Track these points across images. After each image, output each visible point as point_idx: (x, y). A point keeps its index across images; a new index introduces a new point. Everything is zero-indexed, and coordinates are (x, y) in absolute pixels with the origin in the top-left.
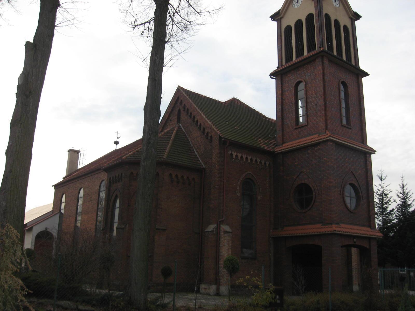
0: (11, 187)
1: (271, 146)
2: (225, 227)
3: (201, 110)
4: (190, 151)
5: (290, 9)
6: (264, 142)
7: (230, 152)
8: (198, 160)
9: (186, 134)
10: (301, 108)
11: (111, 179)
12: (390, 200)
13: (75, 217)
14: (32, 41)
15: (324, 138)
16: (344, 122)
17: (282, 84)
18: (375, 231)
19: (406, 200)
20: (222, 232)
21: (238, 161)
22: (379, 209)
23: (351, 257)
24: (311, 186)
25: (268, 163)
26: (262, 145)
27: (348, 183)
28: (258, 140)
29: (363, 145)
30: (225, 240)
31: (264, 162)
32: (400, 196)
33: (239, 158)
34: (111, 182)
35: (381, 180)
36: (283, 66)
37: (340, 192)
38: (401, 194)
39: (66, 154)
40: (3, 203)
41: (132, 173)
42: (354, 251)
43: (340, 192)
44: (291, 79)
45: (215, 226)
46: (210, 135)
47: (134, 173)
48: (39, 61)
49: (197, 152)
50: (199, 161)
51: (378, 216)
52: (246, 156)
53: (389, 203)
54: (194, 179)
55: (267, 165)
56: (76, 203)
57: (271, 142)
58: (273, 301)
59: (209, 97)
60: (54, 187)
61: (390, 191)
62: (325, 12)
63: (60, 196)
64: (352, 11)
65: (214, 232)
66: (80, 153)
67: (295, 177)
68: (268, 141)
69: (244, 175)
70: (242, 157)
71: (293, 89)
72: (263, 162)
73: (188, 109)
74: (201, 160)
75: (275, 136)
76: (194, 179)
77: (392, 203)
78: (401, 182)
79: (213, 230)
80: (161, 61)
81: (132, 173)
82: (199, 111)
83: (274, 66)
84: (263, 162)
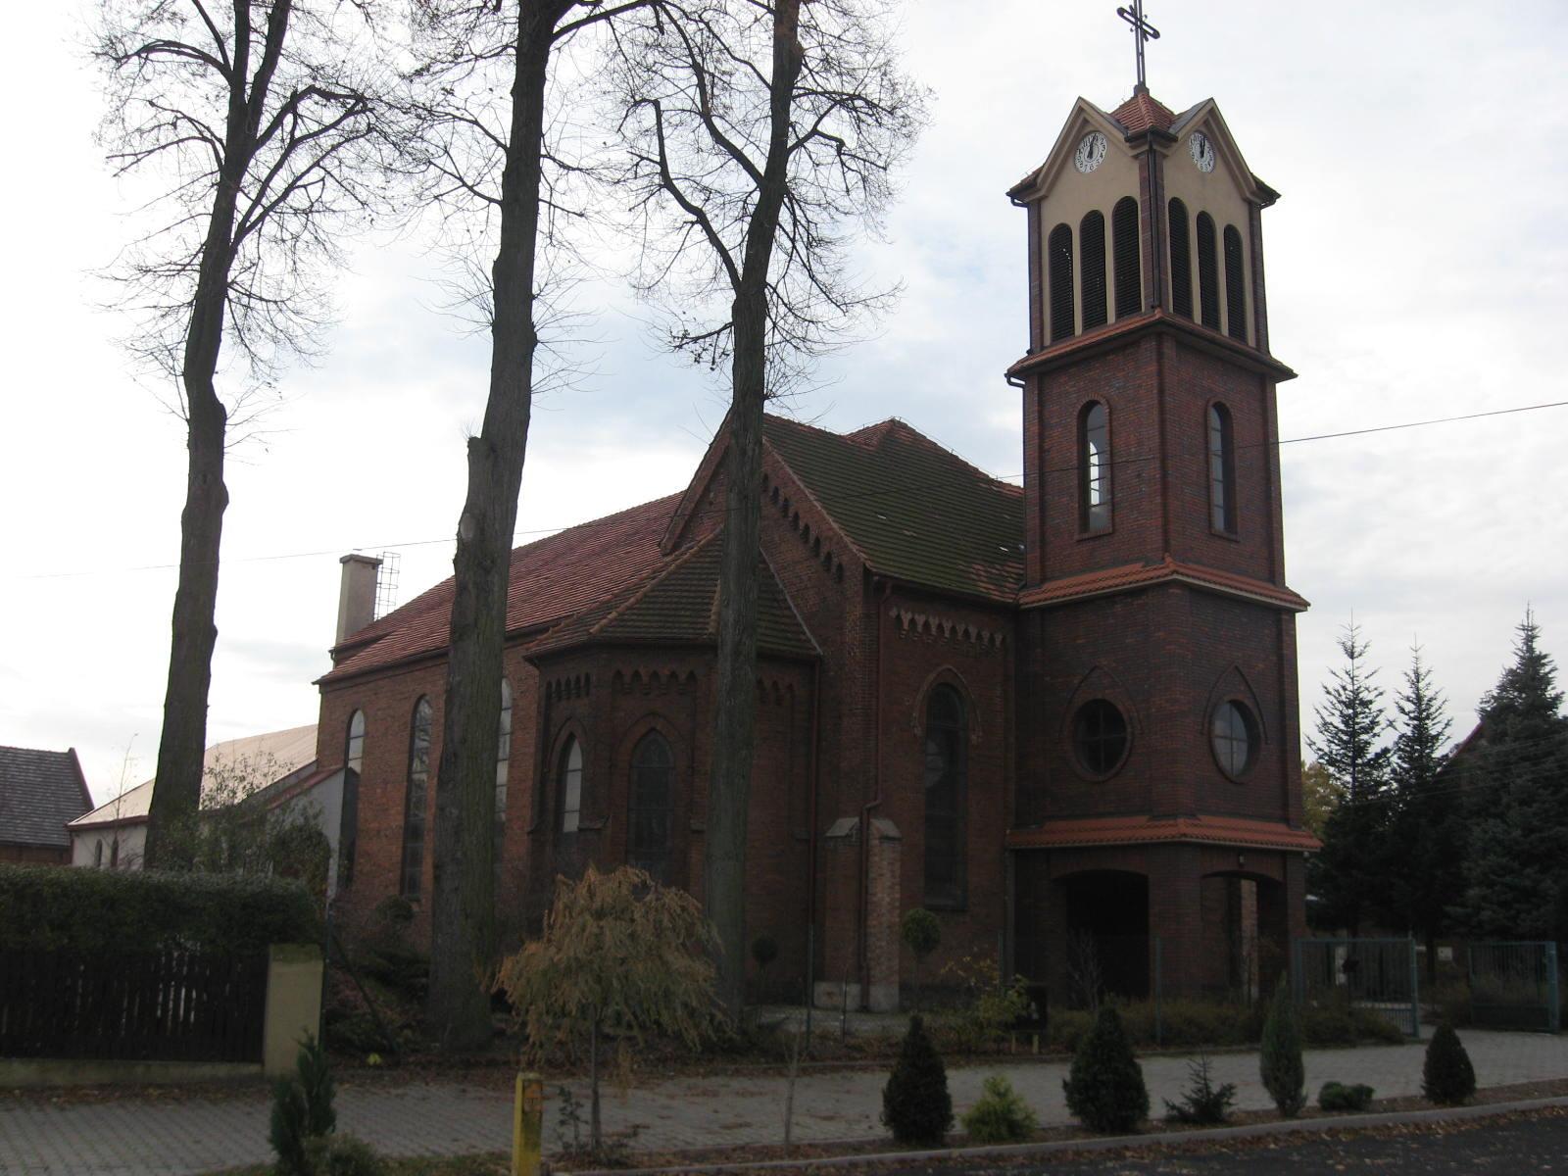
0: (467, 775)
1: (1008, 585)
2: (883, 826)
3: (809, 485)
4: (776, 604)
5: (1068, 175)
6: (988, 572)
7: (893, 613)
10: (1097, 482)
12: (1377, 720)
14: (479, 436)
15: (1159, 577)
16: (1219, 523)
17: (1041, 404)
18: (1300, 833)
19: (1427, 722)
22: (1342, 749)
23: (1240, 902)
24: (1120, 707)
25: (1001, 637)
26: (981, 584)
27: (1226, 698)
28: (972, 570)
29: (1272, 587)
32: (1407, 711)
33: (920, 628)
34: (554, 695)
35: (1352, 656)
36: (1047, 347)
37: (1203, 725)
38: (1410, 703)
39: (336, 573)
40: (453, 811)
41: (619, 674)
42: (1248, 888)
43: (1203, 725)
44: (1070, 392)
48: (505, 486)
49: (797, 606)
50: (805, 634)
51: (1339, 772)
53: (1374, 731)
54: (790, 687)
55: (998, 643)
57: (1007, 572)
58: (1024, 1013)
59: (823, 429)
60: (317, 686)
61: (1376, 692)
62: (1168, 195)
63: (345, 718)
64: (1251, 179)
66: (381, 566)
67: (1076, 682)
68: (997, 569)
69: (931, 677)
70: (926, 625)
71: (1074, 423)
72: (986, 634)
73: (786, 500)
74: (810, 631)
75: (1019, 549)
76: (790, 687)
77: (1383, 729)
78: (1412, 666)
80: (757, 451)
81: (619, 674)
82: (802, 486)
83: (1018, 346)
84: (986, 634)
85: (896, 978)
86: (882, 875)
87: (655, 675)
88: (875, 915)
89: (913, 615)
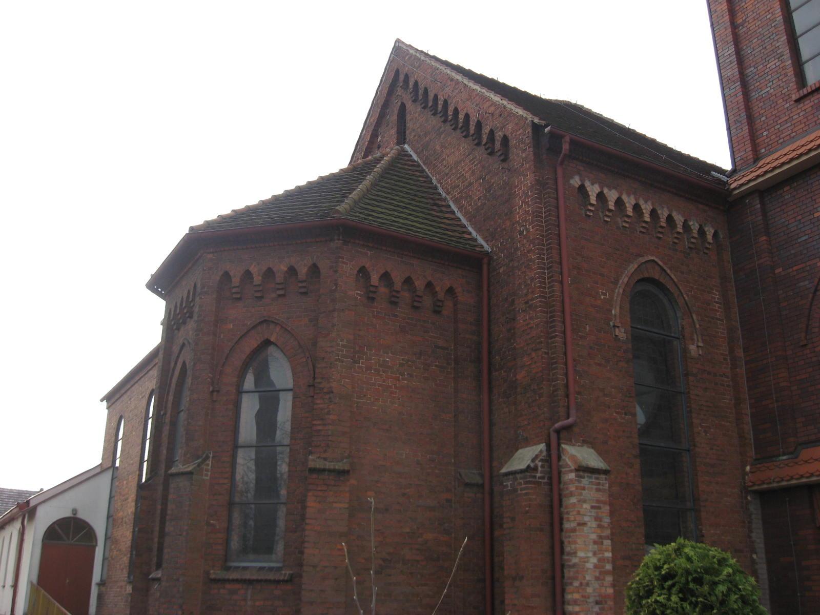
7: (576, 181)
8: (464, 232)
9: (425, 168)
11: (172, 313)
13: (138, 473)
20: (571, 471)
21: (608, 216)
30: (585, 501)
31: (697, 226)
33: (611, 206)
41: (226, 276)
45: (541, 451)
46: (499, 135)
47: (231, 274)
49: (460, 208)
52: (636, 199)
54: (450, 291)
55: (710, 237)
56: (141, 434)
60: (105, 402)
65: (539, 475)
69: (632, 267)
70: (619, 202)
72: (695, 226)
76: (450, 291)
81: (226, 276)
84: (695, 226)
86: (585, 524)
88: (576, 584)
89: (601, 187)
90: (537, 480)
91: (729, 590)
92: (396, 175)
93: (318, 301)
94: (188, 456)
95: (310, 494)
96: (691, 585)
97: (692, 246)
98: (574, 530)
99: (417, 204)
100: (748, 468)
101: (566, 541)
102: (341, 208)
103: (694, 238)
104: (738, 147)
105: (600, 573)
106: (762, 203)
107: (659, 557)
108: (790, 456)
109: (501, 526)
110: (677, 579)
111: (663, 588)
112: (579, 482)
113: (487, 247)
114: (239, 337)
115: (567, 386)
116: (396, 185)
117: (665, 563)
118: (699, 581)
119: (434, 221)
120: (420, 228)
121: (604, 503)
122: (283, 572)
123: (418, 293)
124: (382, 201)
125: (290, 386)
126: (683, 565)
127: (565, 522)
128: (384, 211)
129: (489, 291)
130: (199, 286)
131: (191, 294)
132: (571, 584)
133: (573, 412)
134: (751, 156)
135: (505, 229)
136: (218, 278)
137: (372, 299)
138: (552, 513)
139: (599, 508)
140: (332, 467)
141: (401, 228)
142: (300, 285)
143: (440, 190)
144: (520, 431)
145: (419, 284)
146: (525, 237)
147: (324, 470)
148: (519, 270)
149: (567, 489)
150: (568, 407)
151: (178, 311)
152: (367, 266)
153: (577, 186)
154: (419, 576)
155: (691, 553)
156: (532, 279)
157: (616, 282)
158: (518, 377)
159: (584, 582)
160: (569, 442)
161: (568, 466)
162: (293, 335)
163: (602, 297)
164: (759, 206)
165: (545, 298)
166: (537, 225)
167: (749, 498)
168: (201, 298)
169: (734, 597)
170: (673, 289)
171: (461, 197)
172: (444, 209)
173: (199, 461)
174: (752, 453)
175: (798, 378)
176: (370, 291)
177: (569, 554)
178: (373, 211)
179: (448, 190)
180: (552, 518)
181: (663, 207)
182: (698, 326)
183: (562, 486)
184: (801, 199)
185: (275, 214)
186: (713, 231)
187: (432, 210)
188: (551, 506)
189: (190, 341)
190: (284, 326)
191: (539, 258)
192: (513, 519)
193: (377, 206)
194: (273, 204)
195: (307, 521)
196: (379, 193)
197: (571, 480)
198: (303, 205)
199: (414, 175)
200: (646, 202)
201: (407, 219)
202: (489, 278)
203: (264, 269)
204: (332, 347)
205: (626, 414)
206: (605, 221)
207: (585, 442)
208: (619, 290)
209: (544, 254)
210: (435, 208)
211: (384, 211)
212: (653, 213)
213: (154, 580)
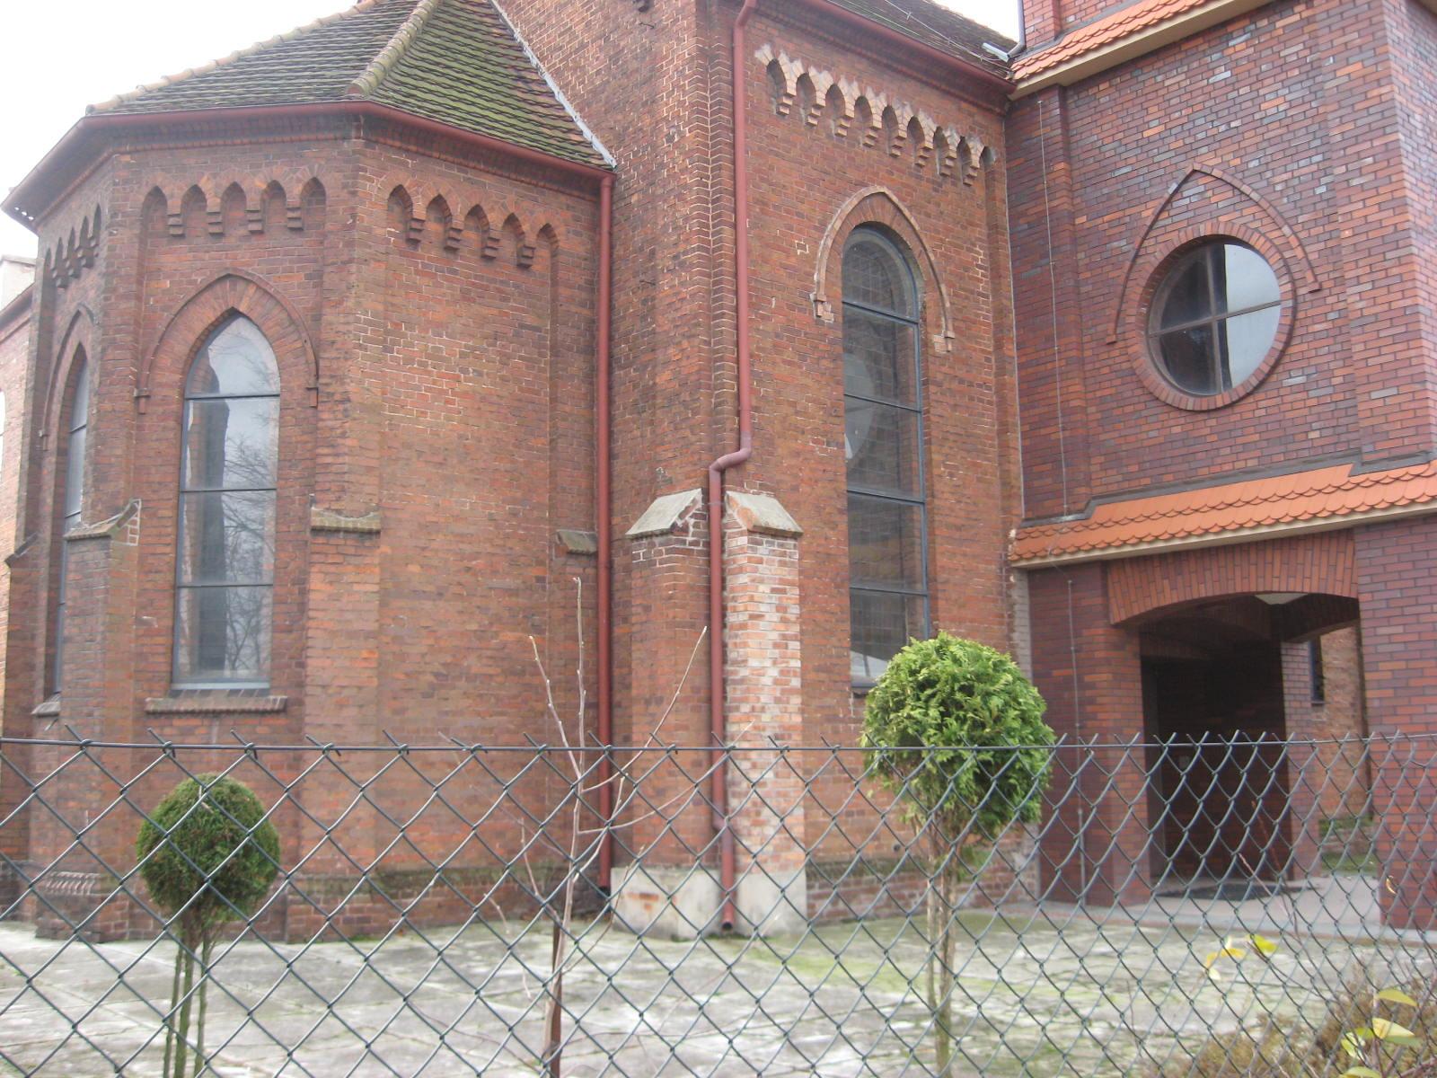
7: (764, 55)
8: (570, 131)
9: (501, 10)
11: (53, 258)
20: (741, 534)
30: (762, 581)
33: (821, 99)
41: (157, 195)
45: (694, 501)
47: (166, 191)
49: (564, 87)
52: (861, 89)
54: (546, 231)
55: (975, 159)
65: (690, 539)
69: (849, 204)
70: (833, 93)
72: (953, 138)
76: (546, 231)
79: (680, 523)
81: (157, 195)
84: (953, 138)
85: (797, 854)
86: (759, 617)
87: (235, 192)
88: (745, 708)
89: (806, 67)
90: (687, 546)
91: (1006, 704)
92: (451, 22)
93: (322, 243)
94: (99, 508)
95: (314, 569)
96: (958, 696)
97: (947, 172)
98: (743, 626)
99: (490, 76)
100: (1013, 533)
101: (730, 642)
102: (365, 79)
103: (951, 159)
104: (1032, 10)
105: (783, 691)
106: (1064, 107)
107: (914, 657)
108: (1078, 516)
109: (626, 620)
110: (938, 686)
111: (919, 699)
112: (754, 550)
113: (609, 159)
114: (182, 303)
115: (738, 397)
116: (453, 41)
117: (922, 666)
118: (968, 690)
119: (519, 108)
120: (497, 121)
121: (791, 584)
122: (272, 697)
123: (493, 234)
124: (431, 71)
125: (275, 389)
126: (949, 669)
127: (729, 613)
128: (433, 88)
129: (611, 234)
130: (106, 211)
131: (91, 225)
132: (737, 709)
133: (746, 439)
134: (1052, 27)
135: (641, 129)
136: (142, 198)
137: (415, 243)
138: (709, 598)
139: (783, 591)
140: (350, 526)
141: (465, 119)
142: (291, 215)
143: (529, 53)
144: (660, 469)
145: (495, 219)
146: (676, 146)
147: (337, 530)
148: (665, 201)
149: (734, 561)
150: (739, 431)
151: (65, 254)
152: (406, 185)
153: (767, 63)
154: (493, 700)
155: (959, 653)
156: (687, 219)
157: (821, 228)
158: (657, 380)
159: (758, 705)
160: (740, 486)
161: (736, 525)
162: (278, 302)
163: (799, 252)
164: (1058, 111)
165: (707, 250)
166: (698, 127)
167: (1012, 579)
168: (111, 234)
169: (1013, 713)
170: (911, 241)
171: (566, 66)
172: (535, 87)
173: (119, 516)
174: (1020, 509)
175: (1099, 394)
176: (412, 229)
177: (735, 662)
178: (416, 88)
179: (542, 54)
180: (709, 608)
181: (904, 105)
182: (948, 305)
183: (725, 556)
184: (1126, 105)
185: (243, 86)
186: (981, 149)
187: (516, 88)
188: (709, 589)
189: (90, 308)
190: (262, 285)
191: (699, 184)
192: (647, 609)
193: (423, 79)
194: (235, 67)
195: (311, 614)
196: (425, 56)
197: (742, 548)
198: (290, 70)
199: (482, 23)
200: (877, 94)
201: (473, 104)
202: (611, 212)
203: (226, 184)
204: (348, 323)
205: (828, 444)
206: (808, 124)
207: (763, 487)
208: (826, 242)
209: (708, 178)
210: (520, 84)
211: (433, 88)
212: (888, 113)
213: (41, 716)
